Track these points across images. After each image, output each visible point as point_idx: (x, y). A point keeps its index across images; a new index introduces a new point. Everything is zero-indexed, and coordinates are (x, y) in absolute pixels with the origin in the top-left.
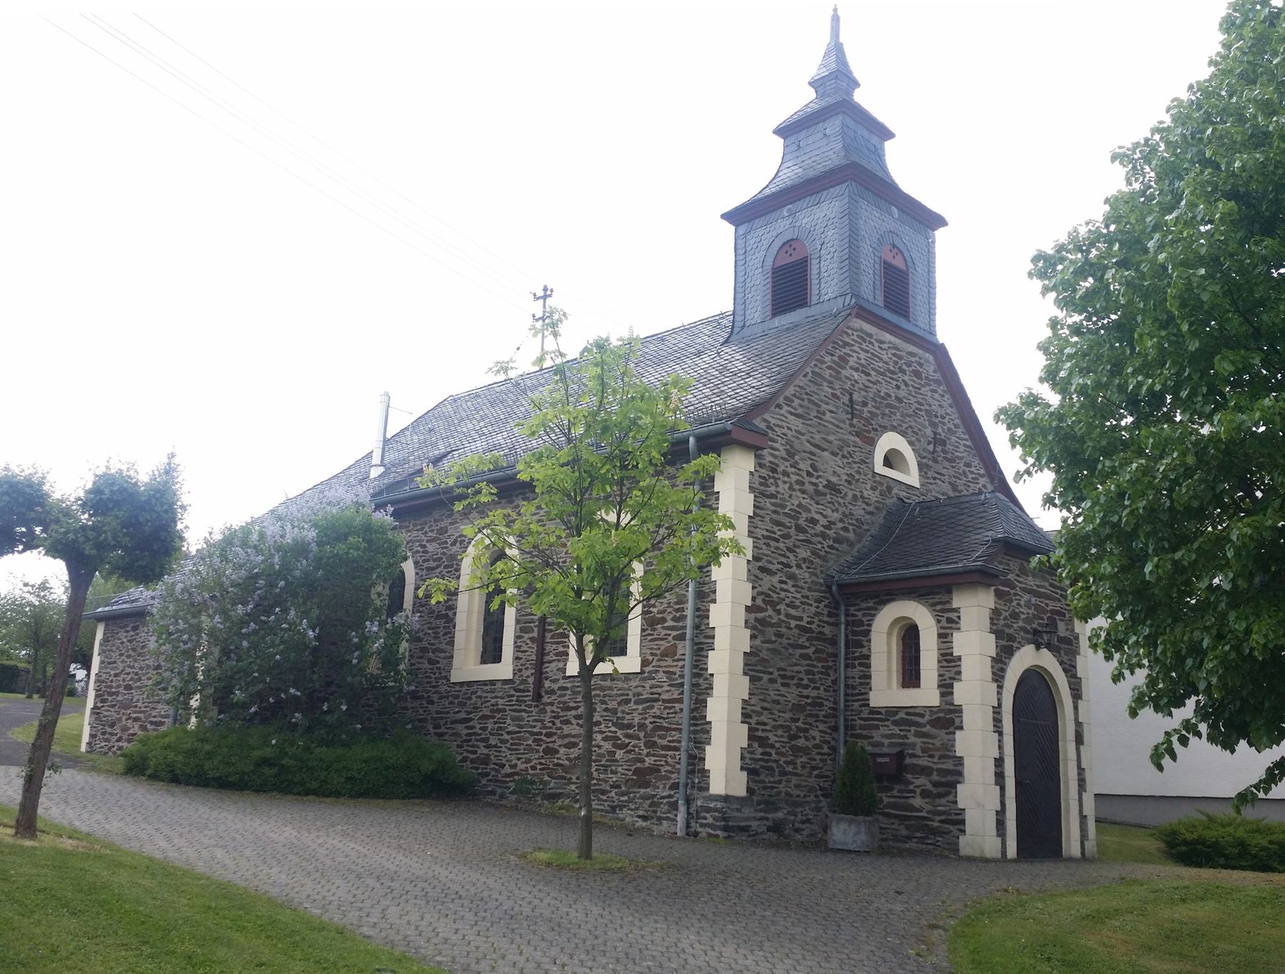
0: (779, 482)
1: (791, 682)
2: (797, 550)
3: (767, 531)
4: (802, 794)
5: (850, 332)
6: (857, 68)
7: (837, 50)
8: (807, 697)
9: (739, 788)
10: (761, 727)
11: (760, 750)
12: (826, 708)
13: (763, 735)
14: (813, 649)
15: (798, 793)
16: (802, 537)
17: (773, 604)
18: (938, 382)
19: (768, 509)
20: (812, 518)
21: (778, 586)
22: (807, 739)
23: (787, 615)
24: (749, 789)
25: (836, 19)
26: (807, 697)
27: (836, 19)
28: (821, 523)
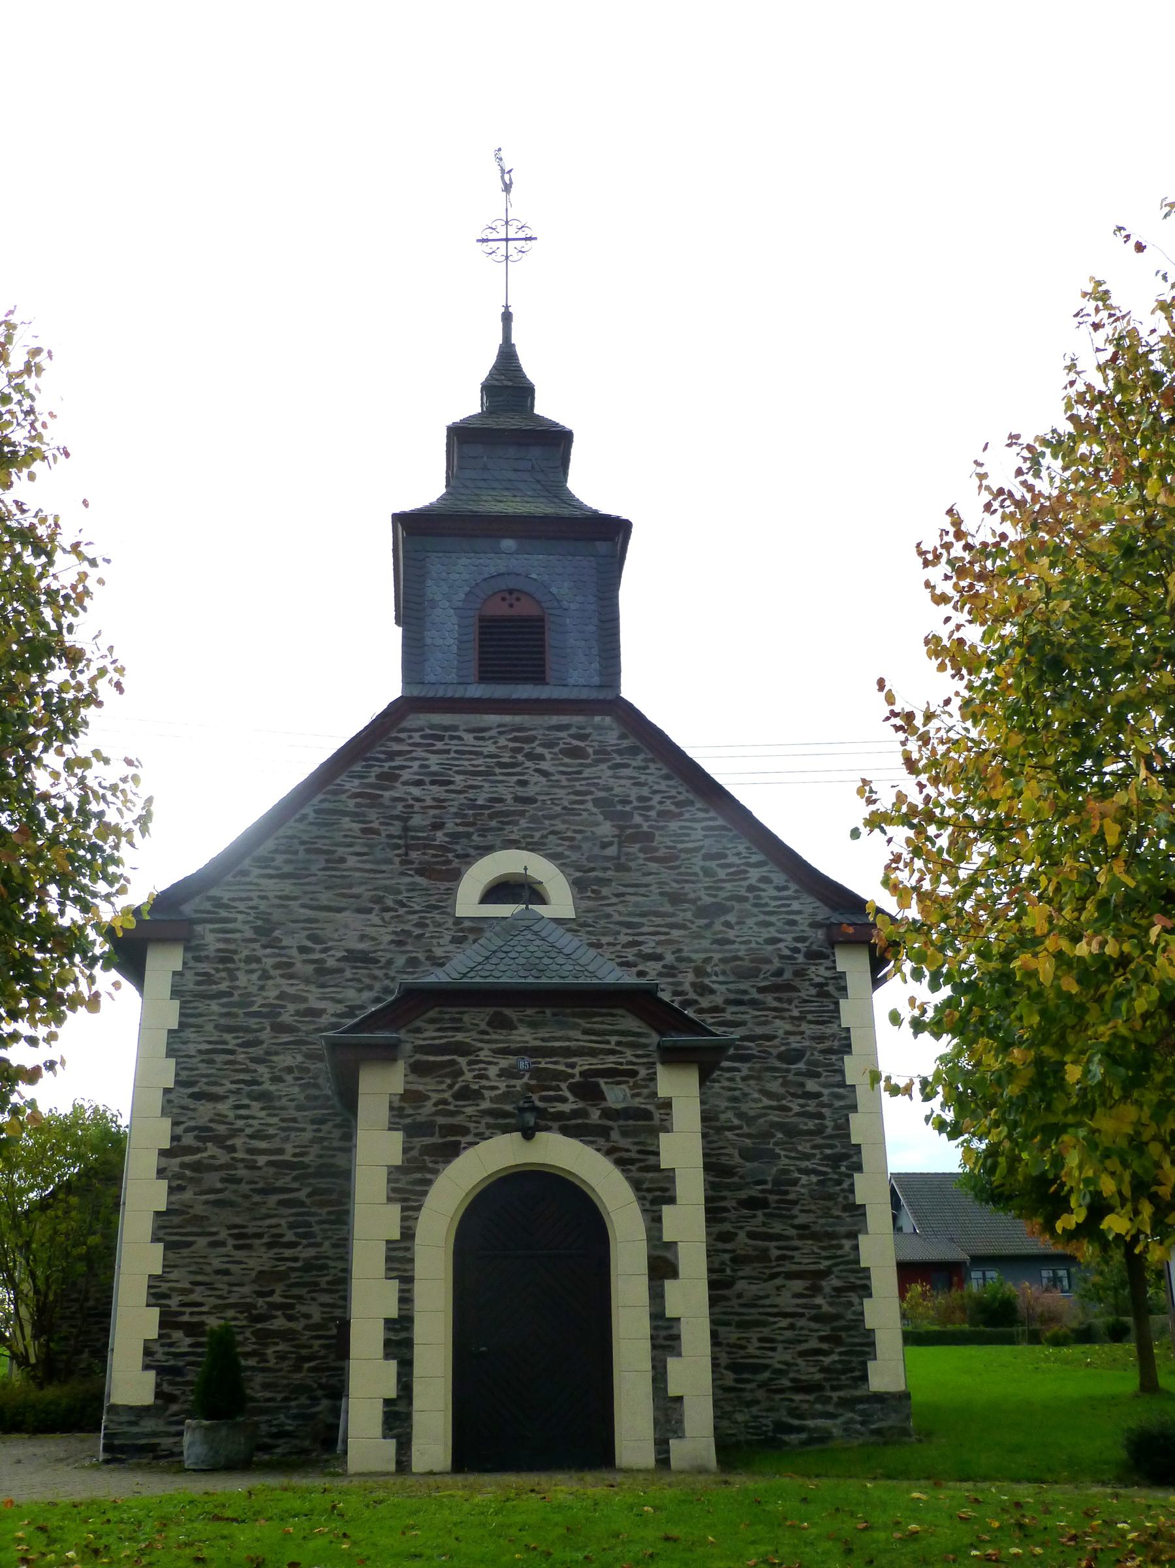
0: (238, 973)
1: (257, 1242)
2: (275, 1058)
3: (210, 1042)
4: (280, 1396)
5: (403, 735)
6: (531, 366)
7: (507, 357)
8: (295, 1259)
9: (146, 1397)
10: (188, 1310)
11: (189, 1341)
12: (332, 1271)
13: (195, 1319)
14: (306, 1190)
15: (268, 1395)
16: (286, 1038)
17: (219, 1141)
18: (633, 751)
19: (213, 1014)
20: (809, 1160)
21: (231, 1114)
22: (290, 1318)
23: (251, 1151)
24: (159, 1394)
25: (507, 318)
26: (295, 1259)
27: (507, 318)
28: (331, 1011)
